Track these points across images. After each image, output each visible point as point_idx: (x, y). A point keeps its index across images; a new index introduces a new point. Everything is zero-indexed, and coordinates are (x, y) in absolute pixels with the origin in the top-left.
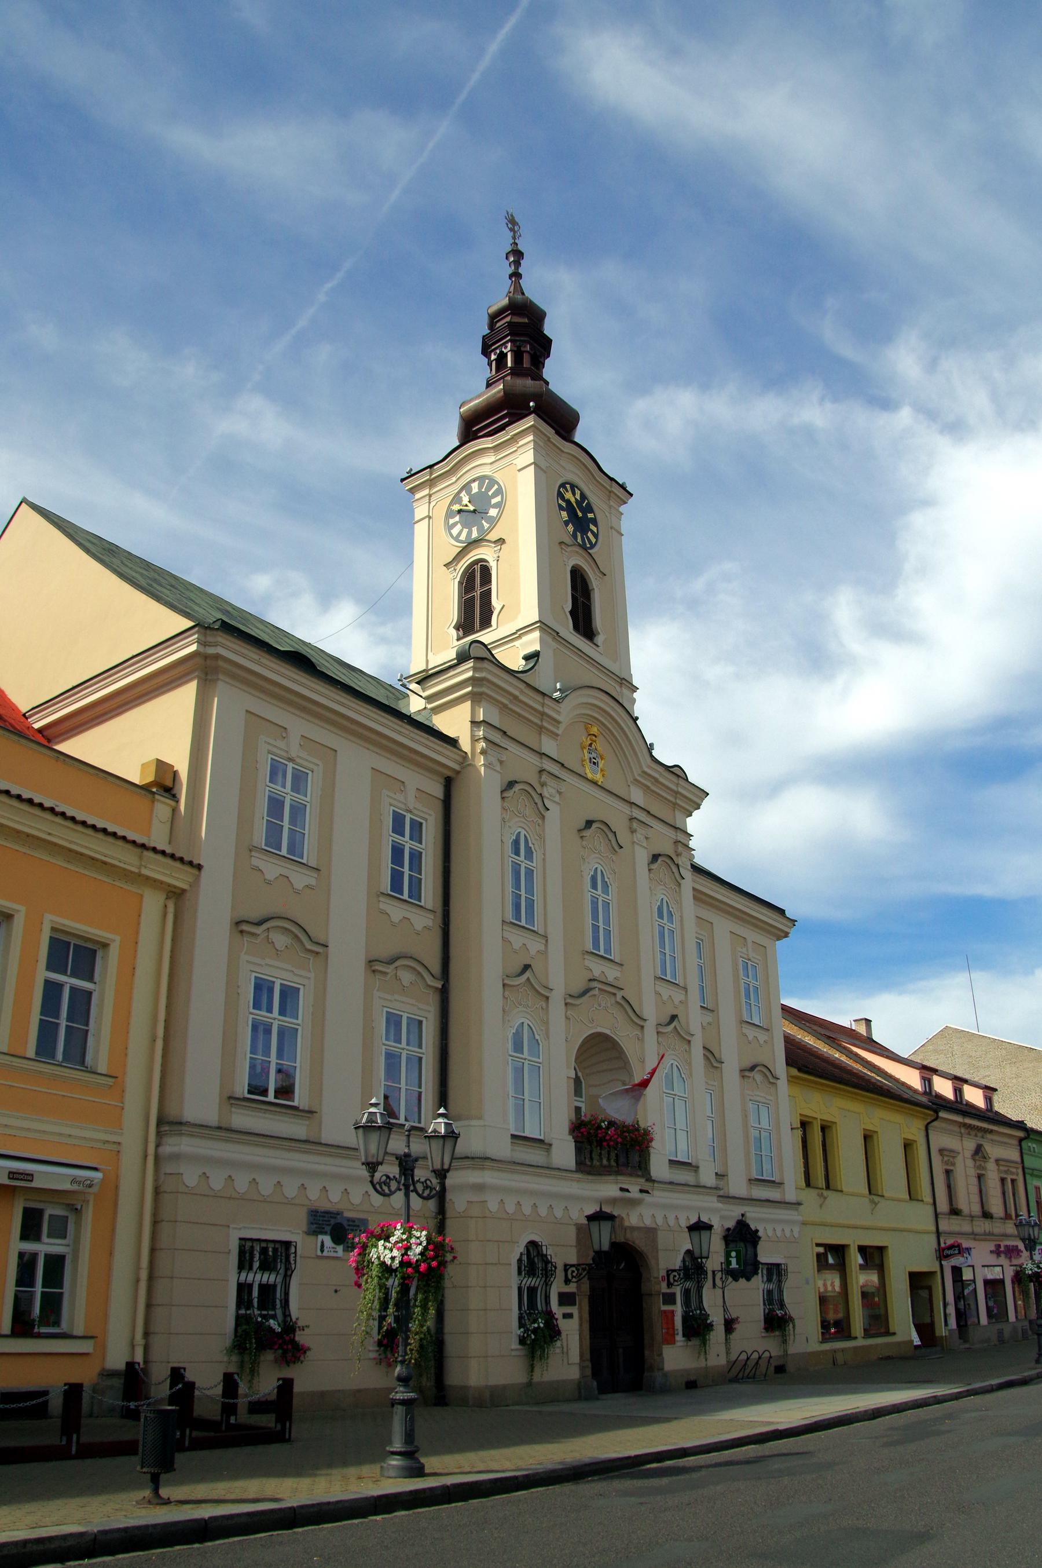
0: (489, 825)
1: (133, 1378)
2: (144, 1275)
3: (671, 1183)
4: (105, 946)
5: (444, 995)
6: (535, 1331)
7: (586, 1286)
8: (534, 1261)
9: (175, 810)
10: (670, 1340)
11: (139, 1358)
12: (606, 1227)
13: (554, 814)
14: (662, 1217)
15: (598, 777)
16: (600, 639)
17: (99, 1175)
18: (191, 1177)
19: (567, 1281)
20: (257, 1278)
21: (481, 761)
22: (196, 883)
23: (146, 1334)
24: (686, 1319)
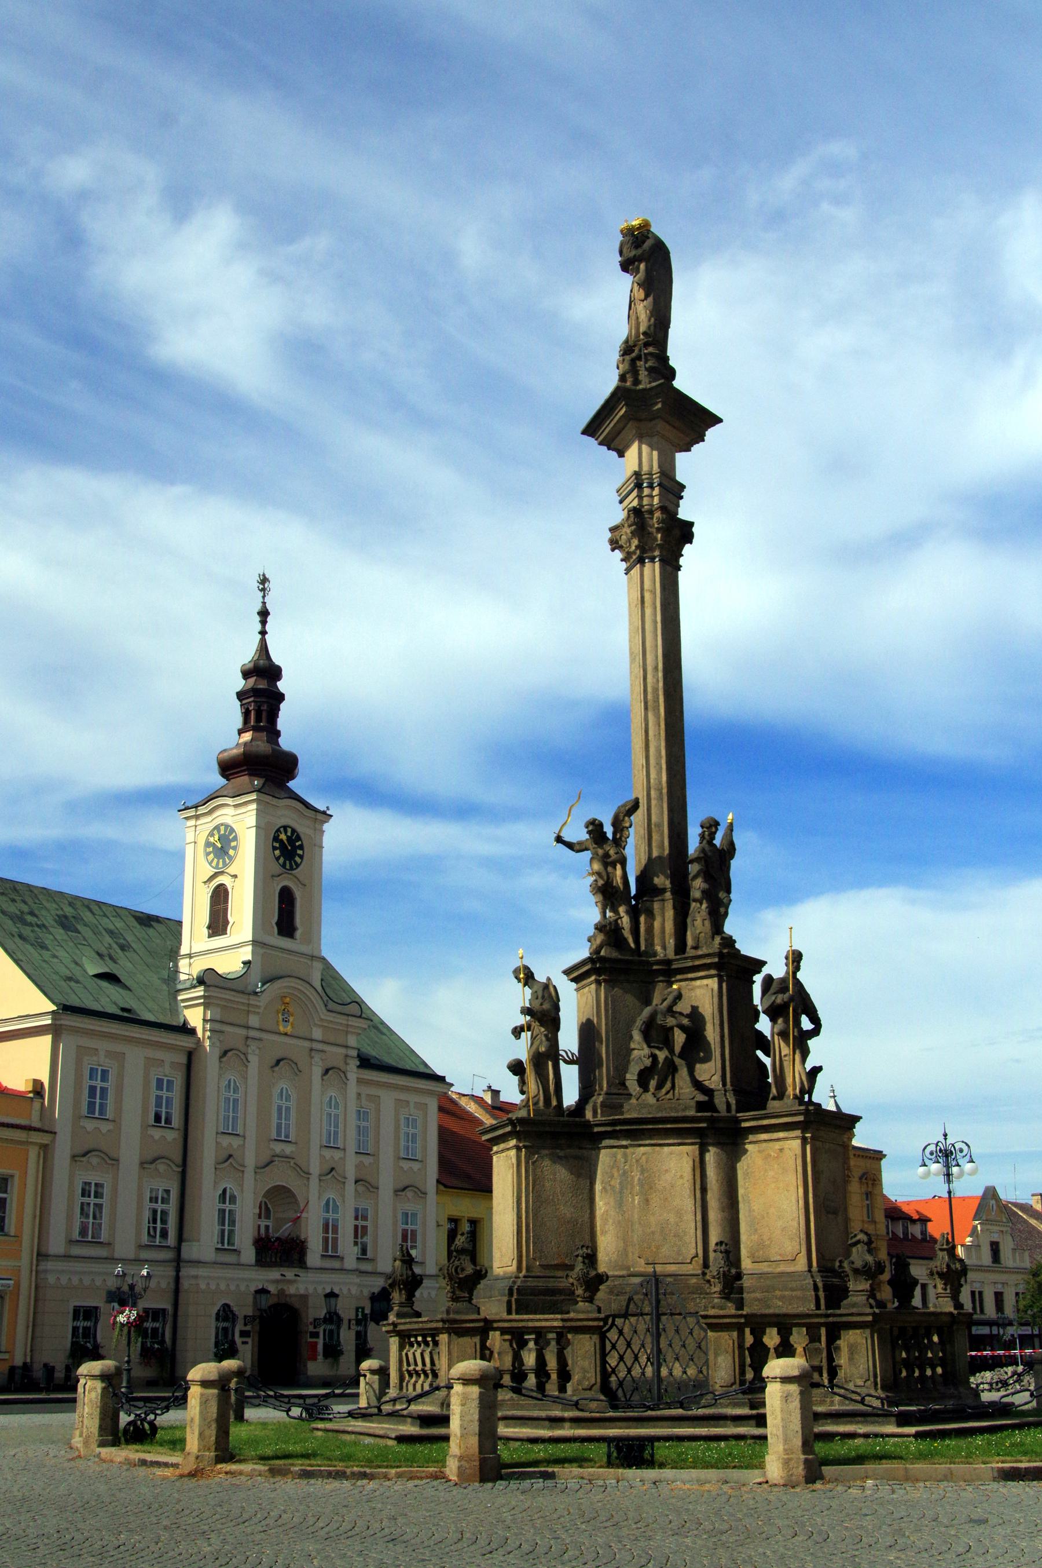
0: (211, 1075)
2: (31, 1324)
3: (321, 1269)
4: (12, 1176)
5: (183, 1174)
6: (223, 1350)
7: (257, 1328)
8: (226, 1314)
9: (43, 1104)
10: (314, 1358)
11: (28, 1360)
12: (264, 1297)
13: (254, 1059)
14: (306, 1285)
15: (289, 1029)
16: (298, 934)
17: (12, 1282)
18: (51, 1279)
19: (245, 1325)
20: (81, 1324)
21: (207, 1043)
22: (53, 1141)
23: (31, 1351)
24: (325, 1346)
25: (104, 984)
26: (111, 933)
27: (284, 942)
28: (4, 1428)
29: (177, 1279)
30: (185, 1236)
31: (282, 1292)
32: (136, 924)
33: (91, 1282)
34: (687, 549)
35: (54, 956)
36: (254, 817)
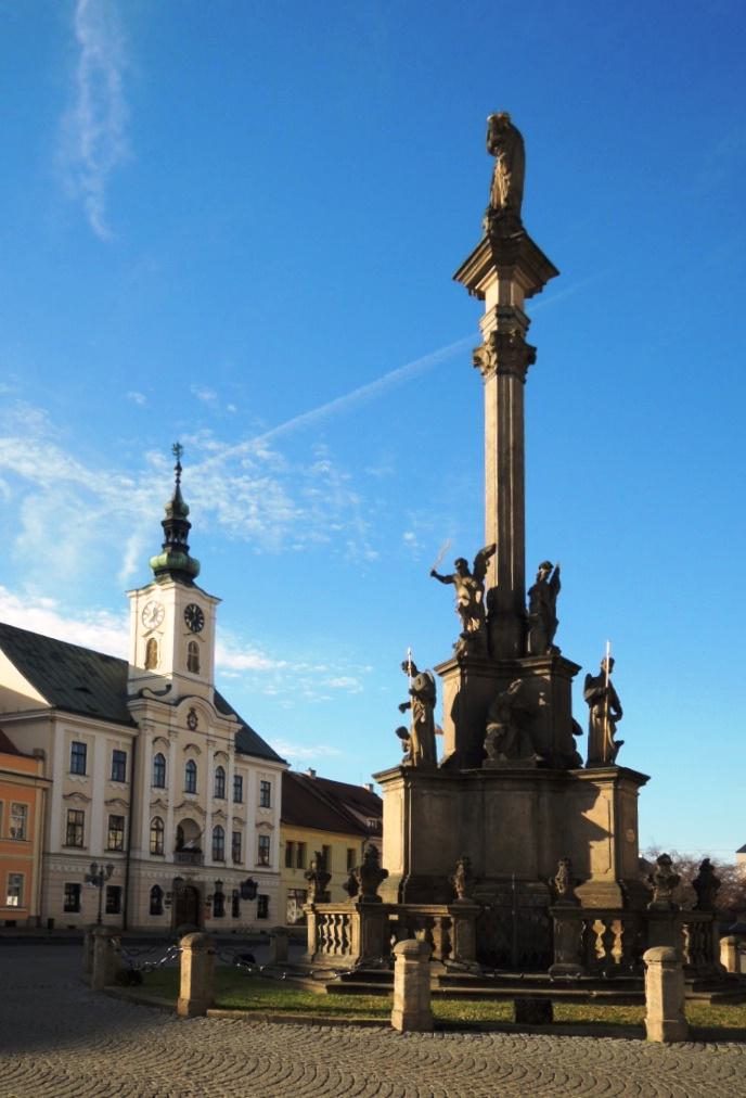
1: (38, 918)
8: (156, 892)
10: (208, 918)
14: (206, 877)
16: (201, 671)
18: (52, 867)
25: (82, 694)
26: (84, 664)
27: (192, 675)
28: (75, 2)
29: (127, 870)
30: (133, 845)
31: (189, 880)
32: (98, 660)
33: (78, 871)
34: (531, 368)
35: (50, 676)
36: (174, 596)
